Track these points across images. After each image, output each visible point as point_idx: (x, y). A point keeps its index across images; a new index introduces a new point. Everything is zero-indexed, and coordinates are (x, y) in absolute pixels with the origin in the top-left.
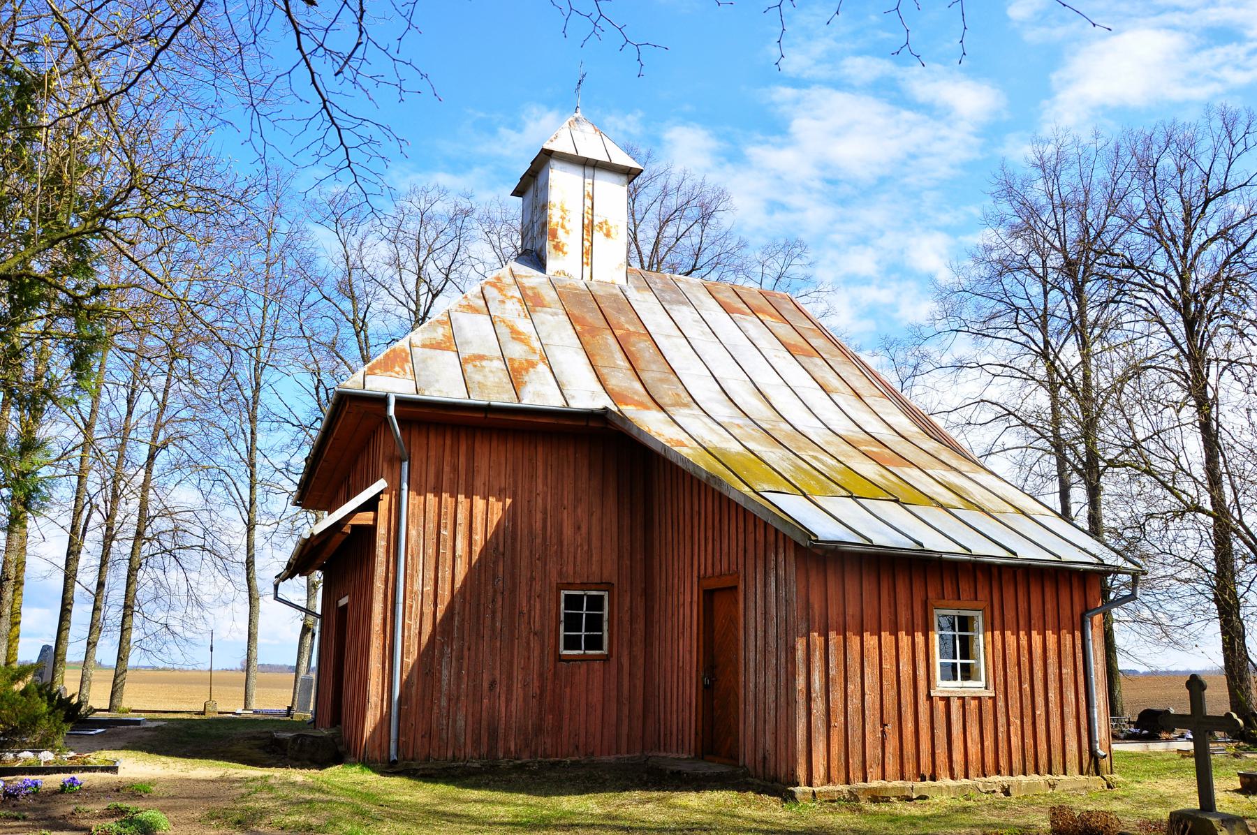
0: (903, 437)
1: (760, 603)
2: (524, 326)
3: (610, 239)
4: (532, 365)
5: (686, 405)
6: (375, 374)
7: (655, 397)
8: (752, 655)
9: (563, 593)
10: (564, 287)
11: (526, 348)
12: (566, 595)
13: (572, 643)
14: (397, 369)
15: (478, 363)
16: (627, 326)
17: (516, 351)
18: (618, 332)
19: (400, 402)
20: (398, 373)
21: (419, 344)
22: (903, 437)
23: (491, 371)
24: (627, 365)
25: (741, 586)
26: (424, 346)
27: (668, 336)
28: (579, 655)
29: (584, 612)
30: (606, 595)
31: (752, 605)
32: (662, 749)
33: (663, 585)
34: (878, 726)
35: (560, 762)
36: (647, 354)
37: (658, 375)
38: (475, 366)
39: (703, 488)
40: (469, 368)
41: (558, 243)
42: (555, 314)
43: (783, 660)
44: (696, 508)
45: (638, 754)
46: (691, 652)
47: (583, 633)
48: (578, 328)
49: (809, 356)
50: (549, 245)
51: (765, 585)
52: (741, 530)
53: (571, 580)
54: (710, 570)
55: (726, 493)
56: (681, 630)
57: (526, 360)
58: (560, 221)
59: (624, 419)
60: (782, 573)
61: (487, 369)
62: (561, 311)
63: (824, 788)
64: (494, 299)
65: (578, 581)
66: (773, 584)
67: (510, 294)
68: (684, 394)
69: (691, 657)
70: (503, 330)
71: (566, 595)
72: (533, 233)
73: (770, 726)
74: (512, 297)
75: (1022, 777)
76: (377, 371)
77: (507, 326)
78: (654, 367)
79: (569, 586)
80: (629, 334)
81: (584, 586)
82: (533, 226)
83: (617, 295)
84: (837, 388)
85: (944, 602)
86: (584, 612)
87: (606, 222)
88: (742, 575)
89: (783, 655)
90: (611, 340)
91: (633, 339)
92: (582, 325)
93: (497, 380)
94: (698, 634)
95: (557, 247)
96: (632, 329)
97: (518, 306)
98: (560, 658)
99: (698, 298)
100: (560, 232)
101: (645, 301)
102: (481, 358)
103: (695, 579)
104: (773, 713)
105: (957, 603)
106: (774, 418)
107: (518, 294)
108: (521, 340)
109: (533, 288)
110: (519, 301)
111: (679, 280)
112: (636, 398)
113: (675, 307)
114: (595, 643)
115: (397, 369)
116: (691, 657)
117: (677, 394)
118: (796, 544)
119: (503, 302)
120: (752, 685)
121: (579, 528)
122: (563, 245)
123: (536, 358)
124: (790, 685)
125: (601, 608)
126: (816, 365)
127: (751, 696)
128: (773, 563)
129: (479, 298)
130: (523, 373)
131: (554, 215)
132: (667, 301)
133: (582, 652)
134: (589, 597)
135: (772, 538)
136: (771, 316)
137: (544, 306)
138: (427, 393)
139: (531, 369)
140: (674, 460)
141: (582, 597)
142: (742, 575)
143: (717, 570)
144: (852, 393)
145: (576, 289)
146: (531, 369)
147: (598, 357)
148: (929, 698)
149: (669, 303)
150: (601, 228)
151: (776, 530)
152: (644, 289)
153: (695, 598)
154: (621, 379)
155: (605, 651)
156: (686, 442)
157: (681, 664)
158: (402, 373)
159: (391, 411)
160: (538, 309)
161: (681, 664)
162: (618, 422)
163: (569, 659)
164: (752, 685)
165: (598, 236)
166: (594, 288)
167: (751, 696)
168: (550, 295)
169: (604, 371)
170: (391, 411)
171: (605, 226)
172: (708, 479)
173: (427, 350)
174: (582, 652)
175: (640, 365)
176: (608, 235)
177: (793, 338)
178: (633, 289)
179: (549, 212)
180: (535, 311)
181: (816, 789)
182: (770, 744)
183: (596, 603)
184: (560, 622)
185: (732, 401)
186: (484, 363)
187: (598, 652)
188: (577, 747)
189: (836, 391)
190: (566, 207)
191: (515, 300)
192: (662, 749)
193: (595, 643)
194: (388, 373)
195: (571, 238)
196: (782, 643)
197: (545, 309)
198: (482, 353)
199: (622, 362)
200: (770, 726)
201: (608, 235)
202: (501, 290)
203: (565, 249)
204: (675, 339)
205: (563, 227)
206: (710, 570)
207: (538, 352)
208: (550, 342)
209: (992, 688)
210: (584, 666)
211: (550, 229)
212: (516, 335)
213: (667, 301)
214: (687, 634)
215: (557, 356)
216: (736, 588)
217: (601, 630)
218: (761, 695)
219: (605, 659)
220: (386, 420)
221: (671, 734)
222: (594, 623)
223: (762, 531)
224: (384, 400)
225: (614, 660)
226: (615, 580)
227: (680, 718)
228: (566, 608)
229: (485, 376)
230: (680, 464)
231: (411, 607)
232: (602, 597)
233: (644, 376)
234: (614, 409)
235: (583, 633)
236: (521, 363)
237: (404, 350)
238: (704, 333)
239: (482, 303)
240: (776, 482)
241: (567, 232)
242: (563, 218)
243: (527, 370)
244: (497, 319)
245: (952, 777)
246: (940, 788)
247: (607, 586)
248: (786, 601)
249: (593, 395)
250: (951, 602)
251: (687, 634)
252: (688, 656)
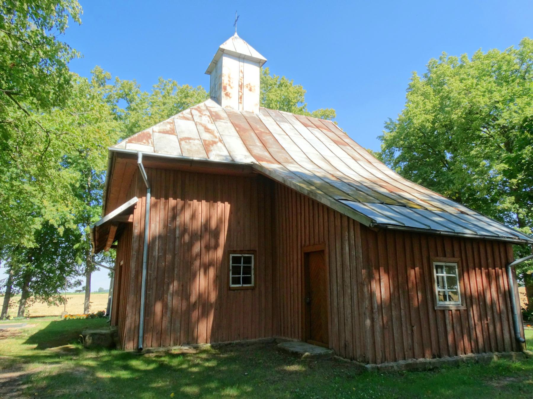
0: (394, 180)
1: (339, 258)
2: (211, 126)
3: (251, 92)
4: (215, 143)
5: (291, 163)
6: (132, 143)
7: (276, 159)
8: (335, 287)
9: (231, 256)
10: (230, 112)
11: (212, 135)
12: (233, 257)
13: (236, 281)
14: (144, 141)
15: (187, 141)
16: (260, 129)
17: (207, 136)
18: (256, 131)
19: (146, 157)
20: (144, 143)
21: (157, 131)
22: (394, 180)
23: (194, 145)
24: (261, 145)
25: (327, 250)
26: (160, 132)
27: (279, 134)
28: (240, 287)
29: (242, 265)
30: (253, 256)
31: (333, 260)
32: (282, 335)
33: (281, 251)
34: (409, 327)
35: (230, 344)
36: (271, 141)
37: (277, 150)
38: (186, 142)
39: (302, 199)
40: (183, 143)
41: (227, 93)
42: (227, 123)
43: (355, 291)
44: (299, 211)
45: (270, 337)
46: (297, 285)
47: (241, 276)
48: (237, 129)
49: (345, 145)
50: (223, 93)
51: (342, 249)
52: (326, 220)
53: (235, 249)
54: (307, 243)
55: (319, 200)
56: (292, 274)
57: (212, 141)
58: (228, 83)
59: (261, 167)
60: (352, 242)
61: (192, 144)
62: (229, 122)
63: (383, 365)
64: (196, 115)
65: (239, 249)
66: (347, 248)
67: (204, 113)
68: (289, 158)
69: (298, 288)
70: (201, 129)
71: (233, 257)
72: (215, 90)
73: (348, 327)
74: (205, 115)
75: (484, 354)
76: (133, 142)
77: (203, 126)
78: (274, 146)
79: (234, 252)
80: (262, 132)
81: (241, 252)
82: (215, 86)
83: (255, 117)
84: (359, 159)
85: (438, 258)
86: (242, 265)
87: (249, 84)
88: (327, 245)
89: (355, 287)
90: (253, 134)
91: (264, 135)
92: (239, 128)
93: (197, 149)
94: (302, 277)
95: (227, 95)
96: (263, 130)
97: (208, 118)
98: (230, 289)
99: (291, 120)
100: (228, 88)
101: (268, 120)
102: (189, 139)
103: (299, 247)
104: (349, 320)
105: (445, 259)
106: (333, 170)
107: (208, 114)
108: (210, 132)
109: (215, 112)
110: (209, 116)
111: (282, 113)
112: (267, 159)
113: (282, 123)
114: (247, 280)
115: (144, 141)
116: (298, 288)
117: (287, 158)
118: (362, 226)
119: (201, 116)
120: (335, 304)
121: (239, 223)
122: (229, 94)
123: (217, 140)
124: (360, 304)
125: (250, 262)
126: (348, 149)
127: (335, 310)
128: (347, 238)
129: (189, 114)
130: (211, 146)
131: (225, 80)
132: (278, 121)
133: (241, 285)
134: (244, 257)
135: (345, 224)
136: (325, 129)
137: (221, 119)
138: (159, 152)
139: (214, 145)
140: (289, 185)
141: (240, 257)
142: (327, 245)
143: (312, 242)
144: (366, 161)
145: (236, 113)
146: (214, 145)
147: (247, 141)
148: (435, 311)
149: (279, 121)
150: (247, 87)
151: (348, 218)
152: (267, 116)
153: (299, 257)
154: (259, 150)
155: (252, 285)
156: (294, 177)
157: (292, 291)
158: (147, 143)
159: (140, 161)
160: (218, 120)
161: (292, 291)
162: (259, 169)
163: (234, 289)
164: (335, 304)
165: (246, 90)
166: (245, 114)
167: (335, 310)
168: (224, 115)
169: (251, 147)
170: (140, 161)
171: (249, 86)
172: (308, 193)
173: (161, 134)
174: (241, 285)
175: (268, 145)
176: (250, 90)
177: (337, 138)
178: (262, 115)
179: (223, 78)
180: (216, 121)
181: (379, 366)
182: (348, 337)
183: (248, 260)
184: (230, 270)
185: (312, 162)
186: (191, 141)
187: (249, 285)
188: (239, 335)
189: (359, 160)
190: (231, 76)
191: (206, 116)
192: (282, 335)
193: (247, 280)
194: (139, 143)
195: (234, 91)
196: (354, 281)
197: (221, 120)
198: (189, 136)
199: (258, 143)
200: (348, 327)
201: (250, 90)
202: (200, 112)
203: (231, 96)
204: (283, 136)
205: (229, 85)
206: (307, 243)
207: (218, 137)
208: (223, 134)
209: (465, 305)
210: (242, 292)
211: (224, 86)
212: (207, 130)
213: (278, 121)
214: (295, 275)
215: (226, 139)
216: (323, 251)
217: (250, 274)
218: (342, 310)
219: (253, 289)
220: (138, 167)
221: (288, 327)
222: (247, 270)
223: (339, 220)
224: (134, 156)
225: (257, 289)
226: (257, 249)
227: (293, 320)
228: (233, 263)
229: (191, 147)
230: (293, 187)
231: (152, 264)
232: (250, 258)
233: (270, 150)
234: (257, 163)
235: (241, 276)
236: (209, 142)
237: (149, 133)
238: (296, 134)
239: (190, 116)
240: (345, 196)
241: (231, 88)
242: (229, 81)
243: (212, 145)
244: (198, 123)
245: (449, 356)
246: (444, 362)
247: (253, 252)
248: (356, 257)
249: (246, 157)
250: (441, 258)
251: (295, 275)
252: (296, 286)
